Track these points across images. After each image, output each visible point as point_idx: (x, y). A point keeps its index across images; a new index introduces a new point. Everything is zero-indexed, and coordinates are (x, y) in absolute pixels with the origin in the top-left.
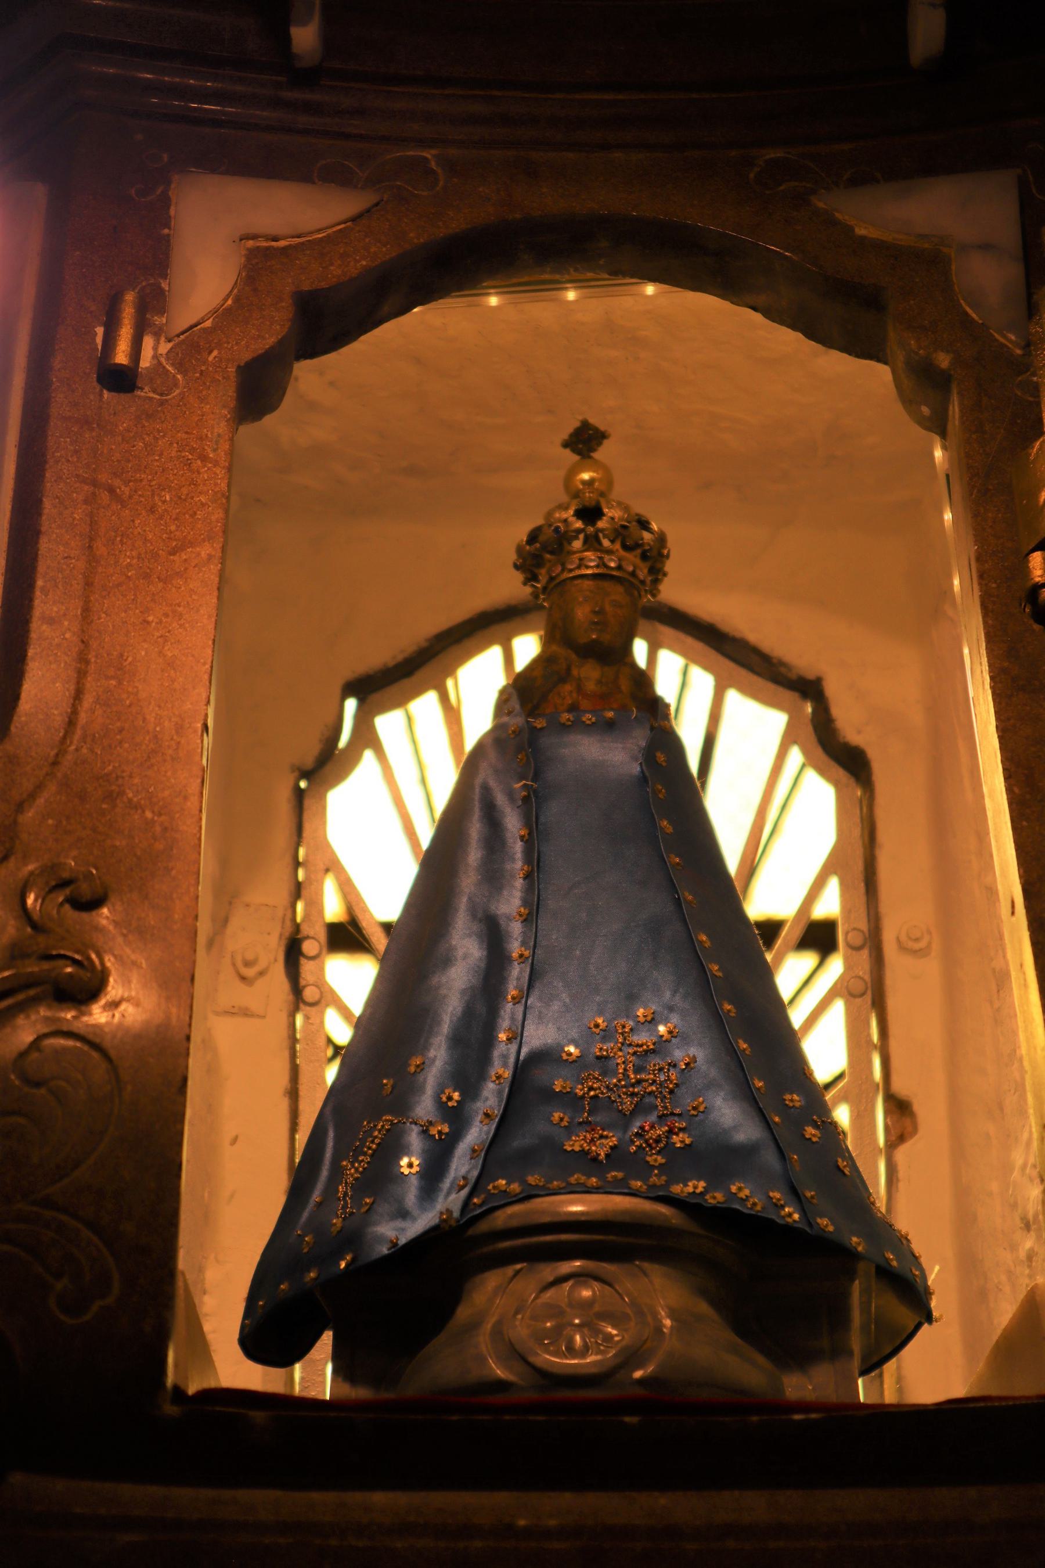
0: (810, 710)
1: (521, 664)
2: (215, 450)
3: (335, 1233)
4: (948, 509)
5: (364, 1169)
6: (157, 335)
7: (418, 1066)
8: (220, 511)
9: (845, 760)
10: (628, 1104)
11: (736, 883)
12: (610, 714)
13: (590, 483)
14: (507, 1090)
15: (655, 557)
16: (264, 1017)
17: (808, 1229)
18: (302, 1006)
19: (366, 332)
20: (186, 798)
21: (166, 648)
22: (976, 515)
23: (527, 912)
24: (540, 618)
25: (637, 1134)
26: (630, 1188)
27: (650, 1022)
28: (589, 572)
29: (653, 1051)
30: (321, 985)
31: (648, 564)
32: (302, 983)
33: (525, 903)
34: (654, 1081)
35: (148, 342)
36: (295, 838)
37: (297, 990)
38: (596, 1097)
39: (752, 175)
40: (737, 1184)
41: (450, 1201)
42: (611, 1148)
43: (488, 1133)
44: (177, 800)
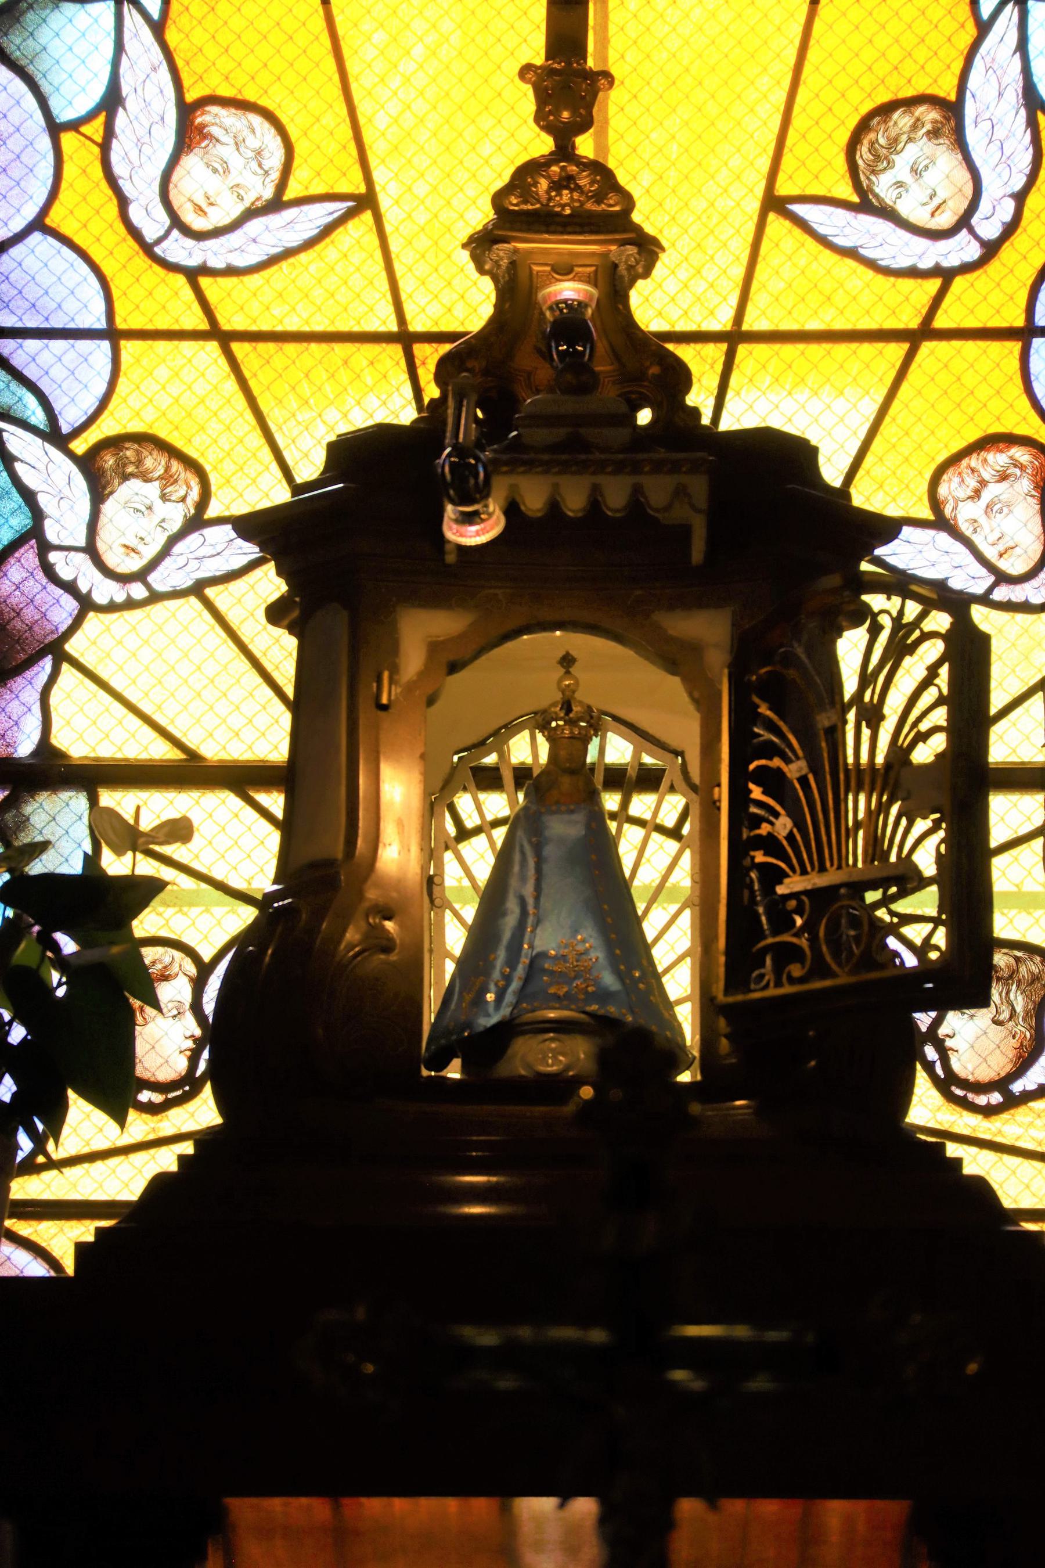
10: (573, 974)
13: (568, 686)
35: (393, 687)
36: (427, 814)
37: (432, 901)
41: (505, 1012)
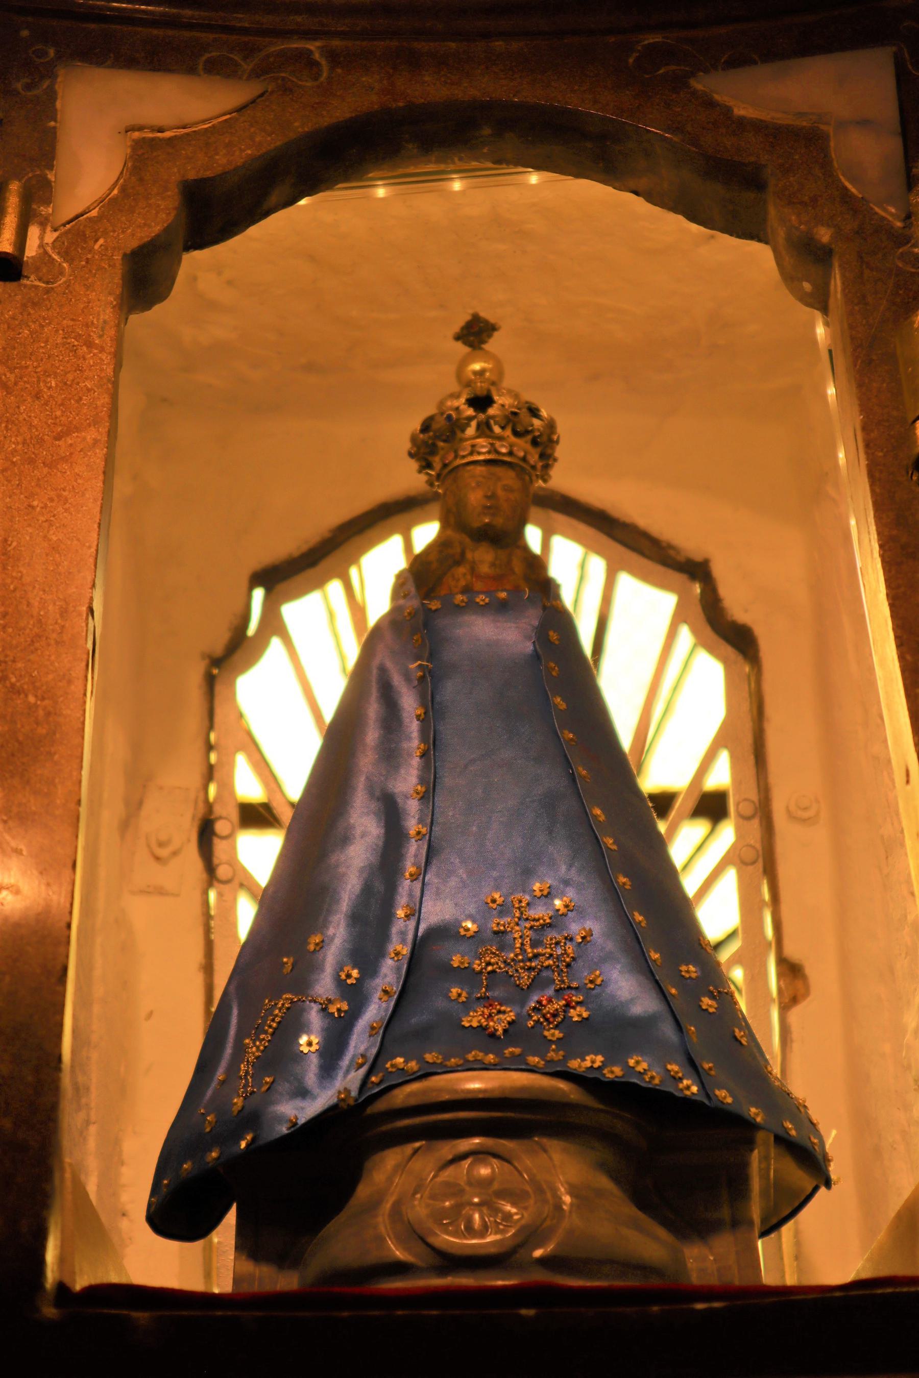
0: (699, 591)
1: (419, 546)
2: (101, 336)
3: (235, 1113)
4: (832, 384)
5: (265, 1047)
6: (43, 224)
7: (317, 944)
8: (106, 396)
9: (733, 638)
10: (525, 979)
11: (630, 758)
12: (503, 595)
13: (481, 373)
14: (405, 966)
15: (545, 444)
16: (177, 895)
17: (706, 1102)
18: (215, 883)
19: (254, 221)
20: (70, 682)
21: (51, 532)
22: (860, 385)
23: (424, 789)
24: (435, 508)
25: (534, 1009)
26: (528, 1064)
27: (546, 896)
28: (481, 458)
29: (550, 925)
30: (233, 862)
31: (539, 450)
32: (216, 861)
33: (422, 780)
34: (551, 955)
35: (34, 232)
37: (210, 868)
38: (493, 971)
39: (631, 60)
40: (635, 1057)
41: (348, 1080)
42: (509, 1023)
43: (386, 1010)
44: (60, 684)
